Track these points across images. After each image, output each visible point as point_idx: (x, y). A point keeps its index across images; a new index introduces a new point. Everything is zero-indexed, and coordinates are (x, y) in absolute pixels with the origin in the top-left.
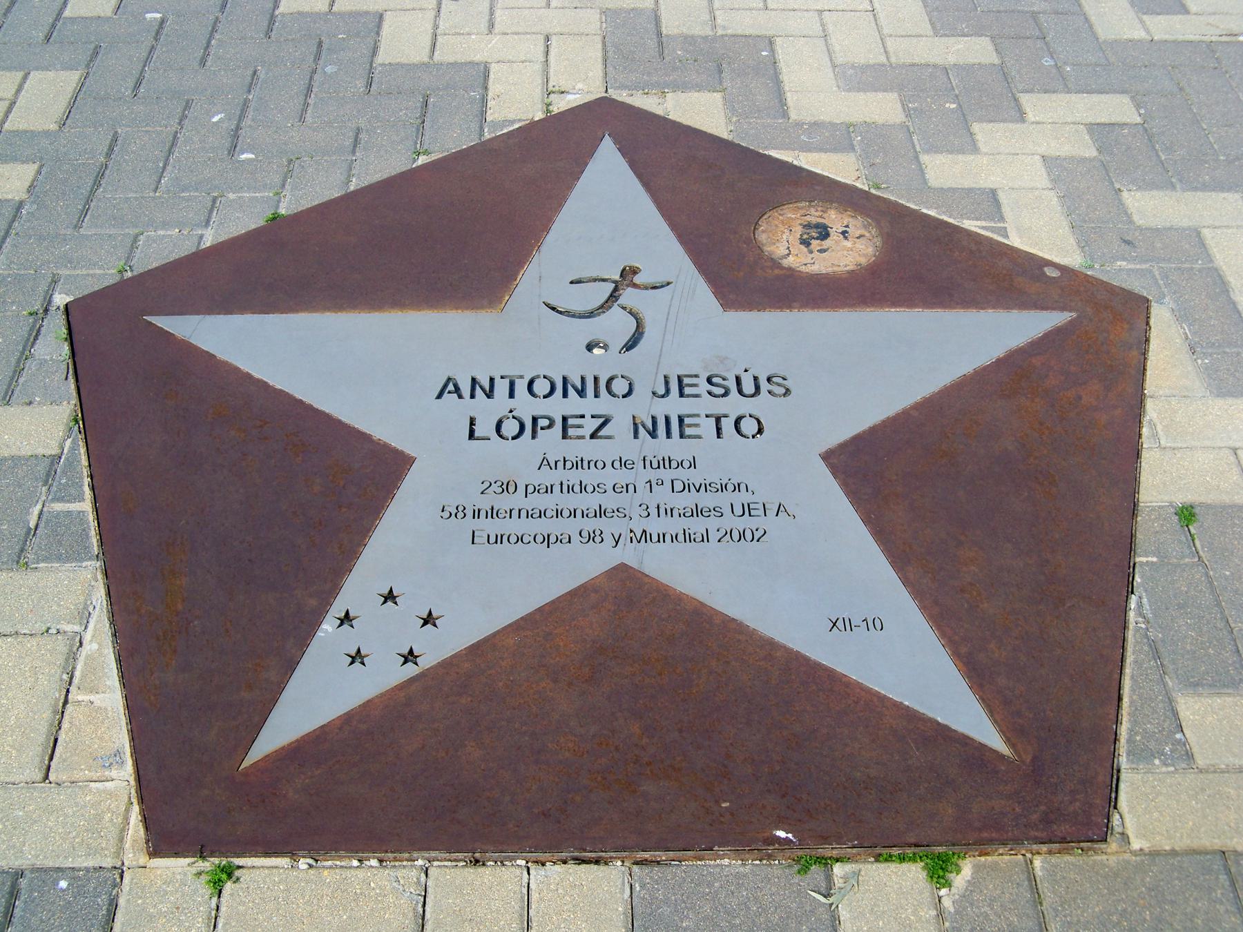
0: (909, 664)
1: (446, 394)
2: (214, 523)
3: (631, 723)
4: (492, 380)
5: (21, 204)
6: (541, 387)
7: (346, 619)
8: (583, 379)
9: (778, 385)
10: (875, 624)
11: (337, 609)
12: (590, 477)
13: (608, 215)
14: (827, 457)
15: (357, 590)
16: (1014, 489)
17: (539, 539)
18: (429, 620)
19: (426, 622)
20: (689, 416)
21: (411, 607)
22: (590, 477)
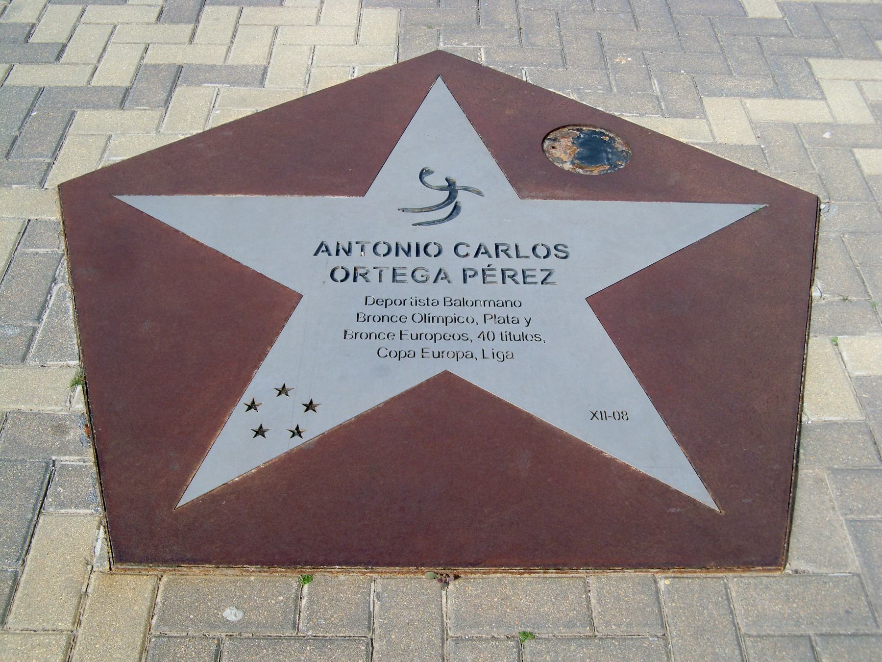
0: (647, 446)
1: (439, 280)
2: (158, 325)
3: (445, 486)
4: (350, 244)
5: (127, 90)
6: (382, 249)
7: (252, 406)
8: (409, 245)
9: (561, 251)
10: (622, 416)
11: (246, 399)
12: (395, 311)
13: (440, 136)
14: (301, 296)
15: (261, 384)
16: (722, 327)
17: (393, 354)
18: (310, 406)
19: (250, 408)
20: (400, 268)
21: (298, 398)
22: (395, 311)
